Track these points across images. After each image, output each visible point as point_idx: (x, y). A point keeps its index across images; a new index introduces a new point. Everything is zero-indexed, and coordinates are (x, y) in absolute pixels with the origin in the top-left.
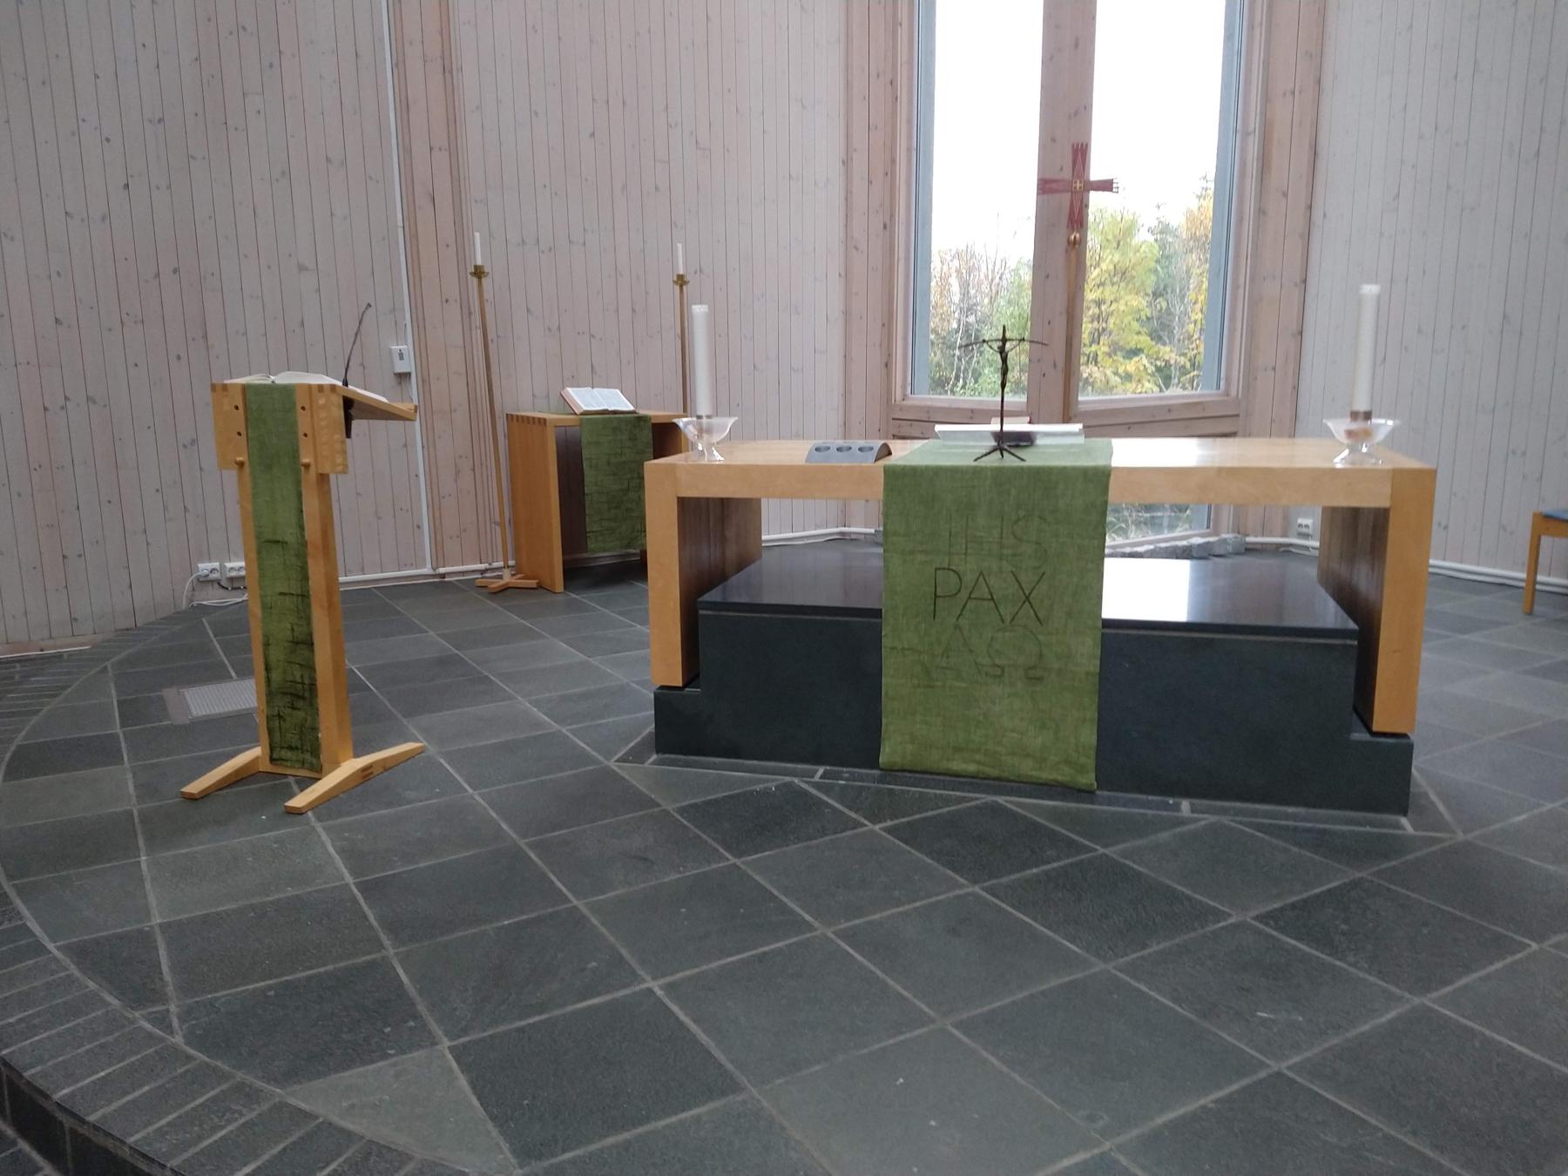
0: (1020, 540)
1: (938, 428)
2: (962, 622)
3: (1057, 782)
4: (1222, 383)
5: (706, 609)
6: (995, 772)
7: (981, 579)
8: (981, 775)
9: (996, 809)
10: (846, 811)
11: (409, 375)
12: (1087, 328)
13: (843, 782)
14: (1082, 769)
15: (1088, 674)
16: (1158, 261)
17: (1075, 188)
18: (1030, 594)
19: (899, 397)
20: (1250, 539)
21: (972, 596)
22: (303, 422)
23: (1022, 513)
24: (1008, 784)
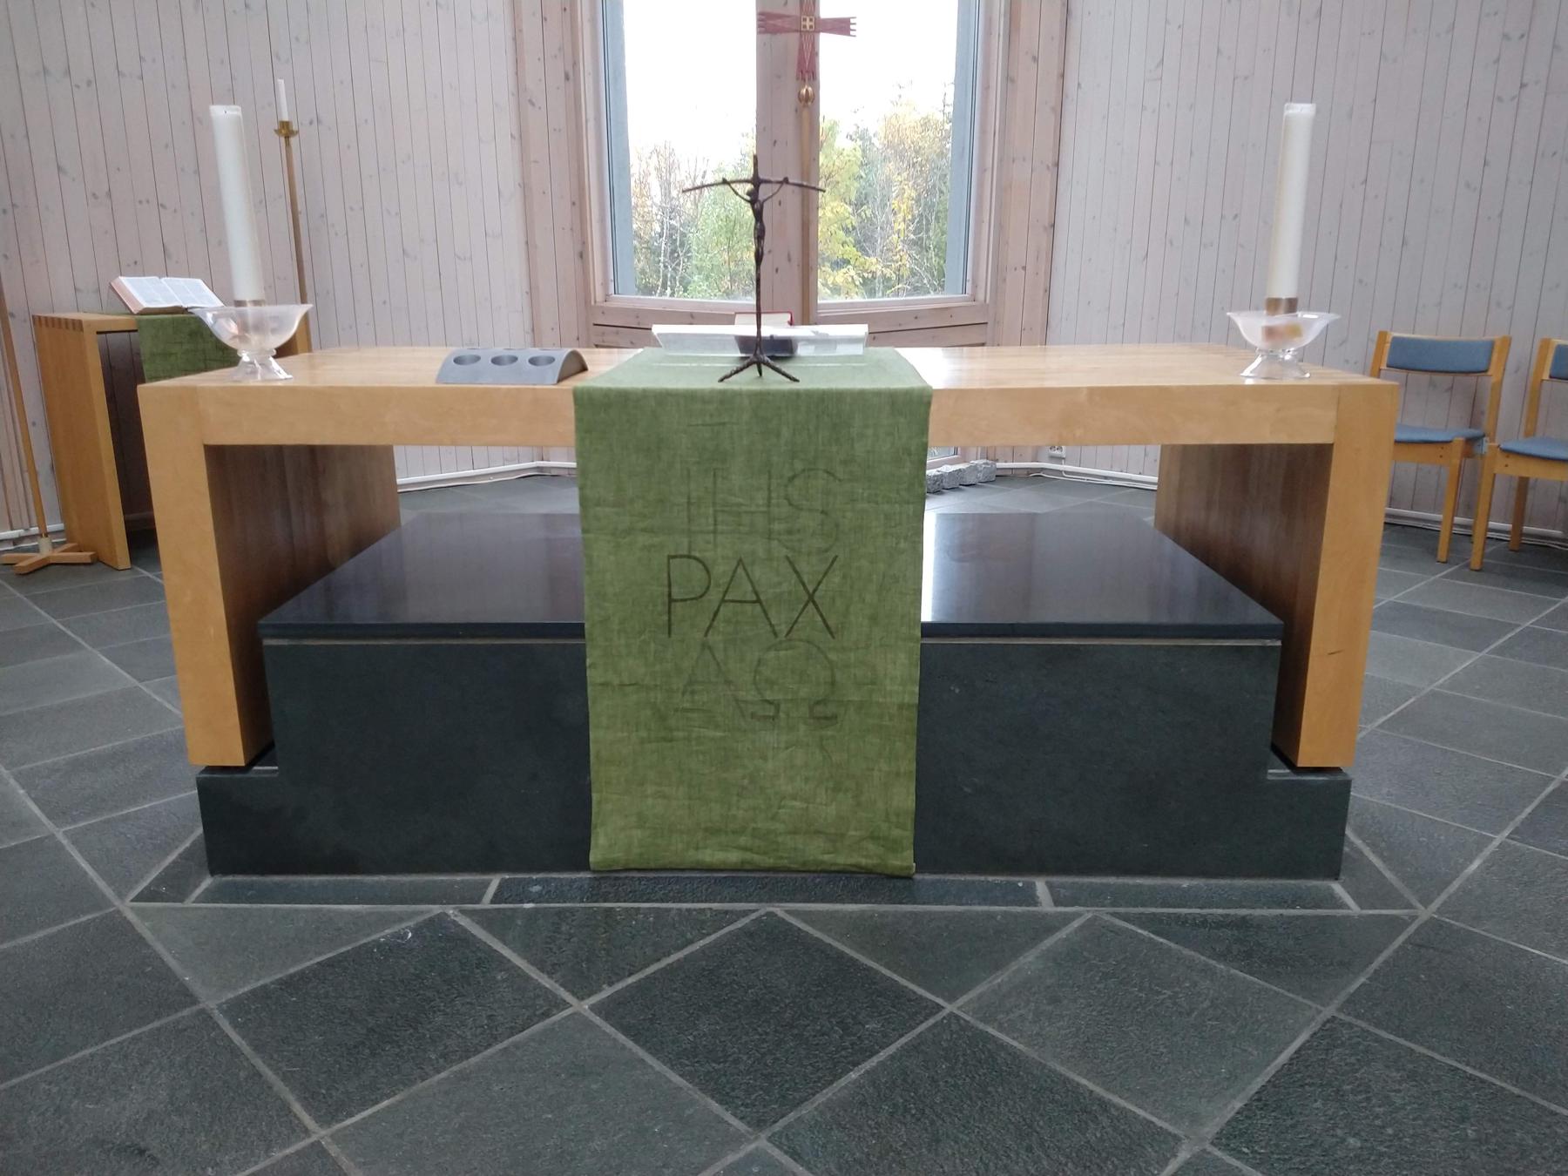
0: (799, 508)
1: (657, 329)
2: (714, 638)
3: (860, 867)
4: (969, 285)
5: (273, 637)
6: (769, 861)
7: (740, 571)
8: (747, 867)
9: (774, 935)
10: (533, 973)
13: (531, 905)
14: (893, 846)
15: (901, 707)
17: (805, 27)
18: (815, 591)
19: (599, 296)
20: (1000, 465)
21: (727, 598)
23: (799, 466)
24: (789, 875)
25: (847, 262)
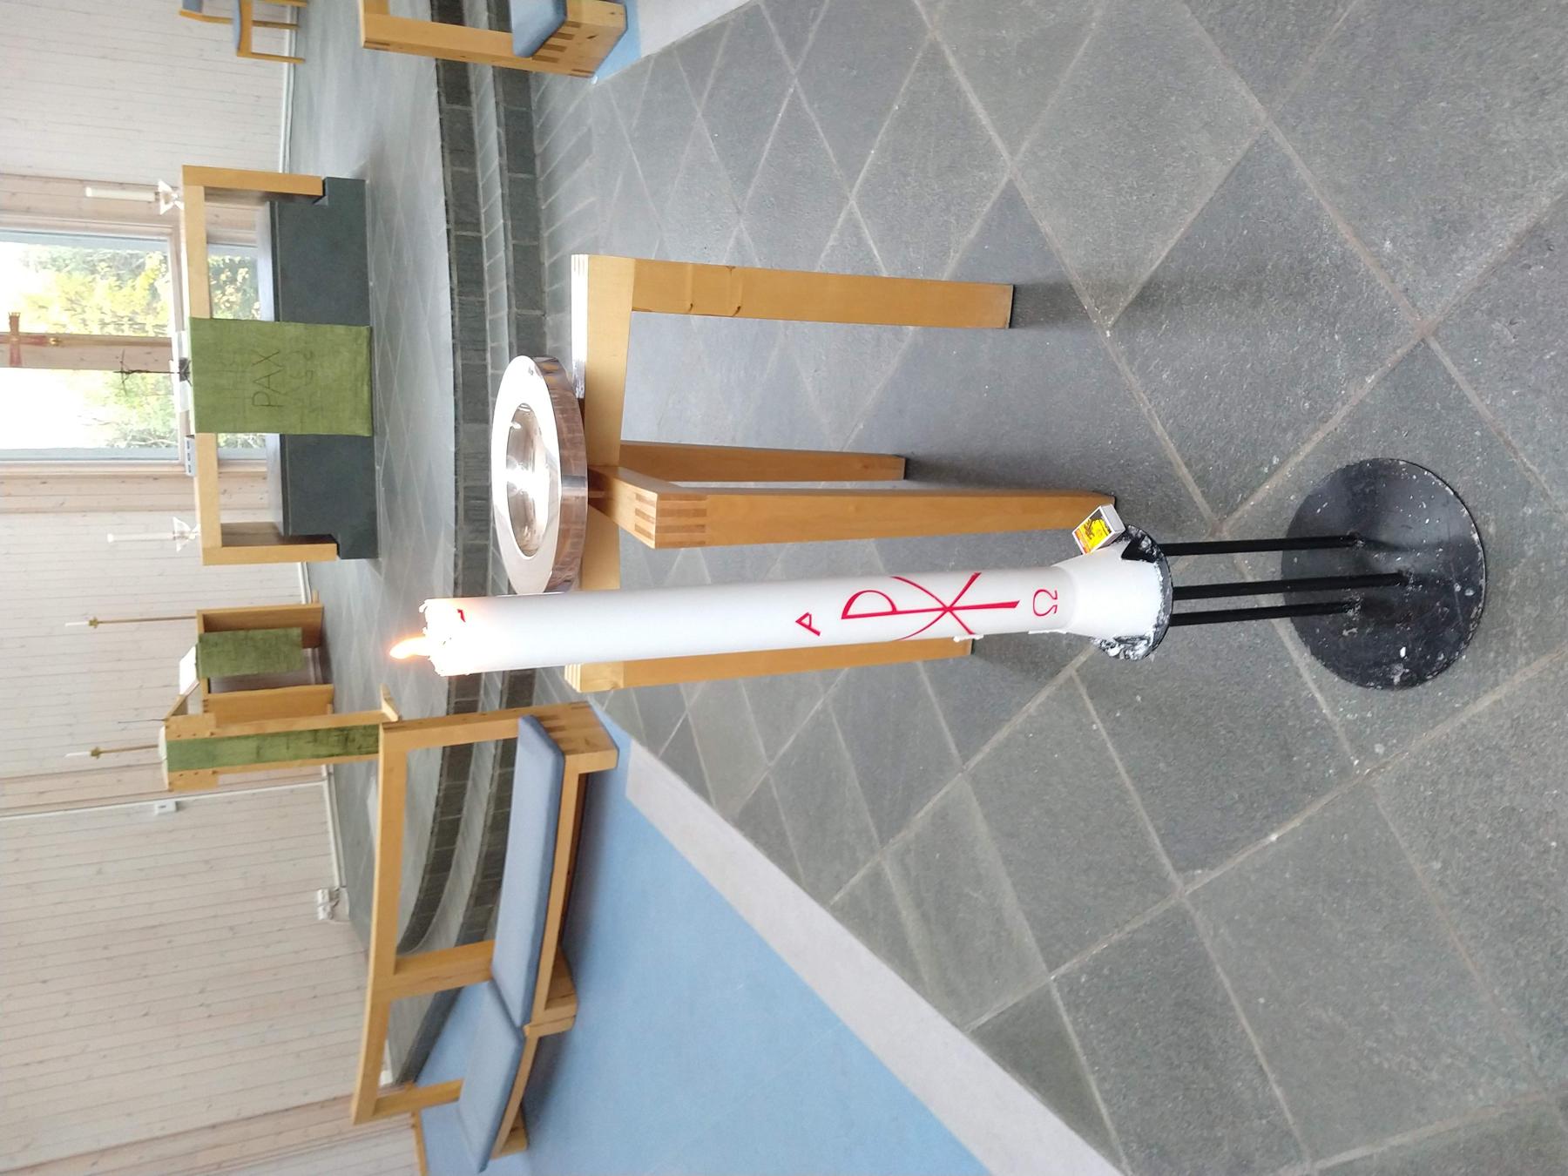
4: (161, 238)
11: (177, 804)
12: (128, 332)
15: (306, 329)
16: (59, 270)
22: (186, 737)
25: (152, 285)
